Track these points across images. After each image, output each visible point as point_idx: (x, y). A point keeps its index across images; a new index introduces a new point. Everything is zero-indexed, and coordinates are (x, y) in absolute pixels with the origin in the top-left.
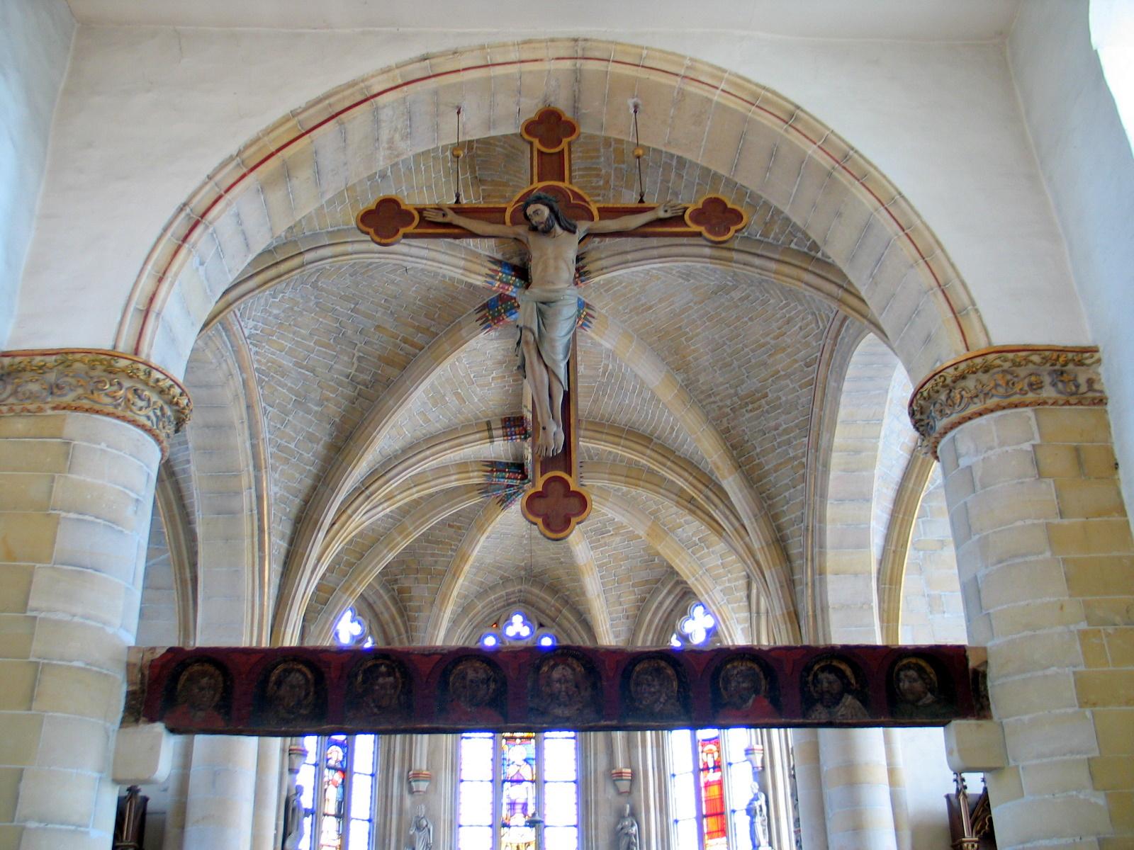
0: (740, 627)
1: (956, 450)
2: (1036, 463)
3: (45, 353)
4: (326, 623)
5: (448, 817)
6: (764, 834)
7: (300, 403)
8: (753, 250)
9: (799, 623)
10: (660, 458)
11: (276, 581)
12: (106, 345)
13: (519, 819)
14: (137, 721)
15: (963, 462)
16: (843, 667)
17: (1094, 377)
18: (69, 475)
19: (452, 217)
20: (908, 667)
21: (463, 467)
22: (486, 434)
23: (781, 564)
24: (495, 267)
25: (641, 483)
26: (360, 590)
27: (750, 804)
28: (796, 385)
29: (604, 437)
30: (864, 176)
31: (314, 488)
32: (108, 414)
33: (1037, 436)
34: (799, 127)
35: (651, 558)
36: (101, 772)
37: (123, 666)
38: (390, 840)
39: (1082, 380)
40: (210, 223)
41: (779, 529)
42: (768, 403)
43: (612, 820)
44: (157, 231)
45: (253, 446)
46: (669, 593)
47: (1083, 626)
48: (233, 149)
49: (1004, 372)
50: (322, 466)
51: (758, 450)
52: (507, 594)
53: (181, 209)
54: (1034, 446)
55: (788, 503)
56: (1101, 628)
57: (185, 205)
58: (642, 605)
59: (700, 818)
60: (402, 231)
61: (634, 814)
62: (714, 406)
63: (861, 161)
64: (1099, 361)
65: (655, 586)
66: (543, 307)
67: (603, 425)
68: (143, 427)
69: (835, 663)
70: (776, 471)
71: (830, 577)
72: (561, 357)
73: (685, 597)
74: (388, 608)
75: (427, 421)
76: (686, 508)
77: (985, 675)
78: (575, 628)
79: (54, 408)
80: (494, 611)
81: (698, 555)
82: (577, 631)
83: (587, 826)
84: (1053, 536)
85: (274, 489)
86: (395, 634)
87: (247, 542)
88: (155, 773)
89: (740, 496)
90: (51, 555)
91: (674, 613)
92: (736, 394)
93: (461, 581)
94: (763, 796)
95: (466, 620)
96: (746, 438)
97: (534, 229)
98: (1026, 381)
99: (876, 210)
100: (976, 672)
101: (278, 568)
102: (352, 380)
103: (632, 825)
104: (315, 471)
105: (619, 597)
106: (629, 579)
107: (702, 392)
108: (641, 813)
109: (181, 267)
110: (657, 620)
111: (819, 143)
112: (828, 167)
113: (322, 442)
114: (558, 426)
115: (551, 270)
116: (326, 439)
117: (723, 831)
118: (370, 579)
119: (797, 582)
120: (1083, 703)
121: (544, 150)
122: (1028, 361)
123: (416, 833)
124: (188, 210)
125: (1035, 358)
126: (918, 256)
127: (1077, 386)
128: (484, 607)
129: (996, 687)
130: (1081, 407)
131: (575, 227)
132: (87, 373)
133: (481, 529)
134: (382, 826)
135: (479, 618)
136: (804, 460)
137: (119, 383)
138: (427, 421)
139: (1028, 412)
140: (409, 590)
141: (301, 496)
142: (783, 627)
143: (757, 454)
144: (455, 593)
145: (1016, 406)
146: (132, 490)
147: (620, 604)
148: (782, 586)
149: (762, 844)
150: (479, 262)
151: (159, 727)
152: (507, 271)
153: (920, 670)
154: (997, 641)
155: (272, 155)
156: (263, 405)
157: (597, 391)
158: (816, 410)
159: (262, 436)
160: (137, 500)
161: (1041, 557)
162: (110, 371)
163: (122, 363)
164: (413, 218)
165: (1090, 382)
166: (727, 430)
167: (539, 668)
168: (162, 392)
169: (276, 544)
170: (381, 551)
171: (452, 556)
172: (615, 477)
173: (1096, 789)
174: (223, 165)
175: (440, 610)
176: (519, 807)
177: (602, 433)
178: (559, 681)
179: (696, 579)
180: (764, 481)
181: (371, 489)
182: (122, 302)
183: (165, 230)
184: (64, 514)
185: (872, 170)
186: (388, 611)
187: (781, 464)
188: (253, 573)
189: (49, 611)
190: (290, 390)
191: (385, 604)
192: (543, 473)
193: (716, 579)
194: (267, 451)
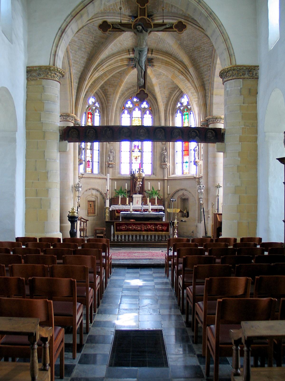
0: (195, 103)
1: (226, 86)
2: (241, 92)
3: (36, 67)
4: (86, 101)
5: (118, 149)
6: (197, 156)
7: (80, 49)
8: (194, 22)
9: (206, 106)
10: (174, 60)
11: (75, 94)
12: (47, 64)
13: (136, 150)
14: (62, 140)
15: (227, 89)
16: (197, 131)
17: (257, 72)
18: (45, 93)
19: (120, 27)
20: (209, 132)
21: (122, 60)
22: (128, 53)
23: (203, 91)
24: (130, 18)
25: (169, 66)
26: (95, 92)
27: (194, 149)
28: (209, 46)
29: (159, 54)
30: (215, 19)
31: (84, 70)
32: (51, 80)
33: (242, 86)
34: (201, 4)
35: (173, 83)
36: (57, 150)
37: (59, 130)
39: (254, 73)
40: (66, 32)
41: (203, 82)
42: (202, 50)
43: (161, 151)
44: (55, 35)
45: (68, 61)
46: (178, 91)
47: (243, 126)
48: (69, 13)
49: (238, 71)
50: (86, 64)
51: (199, 61)
52: (134, 90)
53: (59, 29)
54: (241, 88)
55: (206, 75)
56: (246, 127)
57: (60, 28)
58: (170, 94)
60: (108, 30)
61: (166, 149)
62: (188, 49)
63: (214, 15)
64: (259, 69)
65: (174, 89)
66: (140, 52)
67: (159, 51)
68: (57, 81)
69: (195, 130)
70: (203, 67)
71: (214, 96)
72: (143, 64)
73: (181, 95)
74: (102, 95)
75: (112, 50)
76: (181, 73)
77: (224, 134)
78: (152, 99)
79: (40, 79)
80: (130, 94)
81: (185, 83)
82: (153, 101)
83: (154, 152)
84: (241, 107)
85: (74, 71)
86: (104, 101)
87: (68, 85)
89: (193, 73)
90: (44, 110)
91: (179, 97)
92: (193, 47)
93: (122, 87)
94: (198, 147)
95: (123, 98)
96: (196, 58)
97: (138, 31)
98: (242, 73)
99: (216, 28)
100: (223, 133)
101: (76, 91)
102: (93, 42)
103: (165, 152)
104: (84, 66)
105: (164, 92)
106: (167, 87)
107: (185, 46)
109: (61, 43)
110: (174, 99)
111: (205, 9)
112: (207, 16)
113: (85, 58)
114: (143, 79)
115: (142, 42)
116: (86, 57)
117: (188, 155)
118: (98, 88)
119: (207, 96)
120: (240, 141)
121: (141, 7)
122: (243, 69)
124: (61, 29)
125: (244, 68)
126: (224, 41)
127: (253, 75)
128: (127, 94)
129: (226, 137)
130: (253, 79)
131: (147, 30)
132: (45, 71)
133: (127, 74)
135: (126, 97)
136: (210, 65)
137: (52, 73)
138: (112, 50)
139: (241, 80)
140: (107, 89)
141: (81, 72)
142: (202, 107)
143: (199, 62)
144: (120, 91)
145: (239, 79)
146: (56, 95)
147: (164, 94)
148: (203, 97)
150: (126, 17)
151: (67, 142)
152: (133, 19)
153: (212, 133)
154: (227, 128)
155: (78, 13)
156: (71, 50)
157: (158, 42)
158: (213, 53)
159: (70, 58)
160: (58, 97)
161: (238, 112)
162: (50, 70)
163: (52, 68)
164: (111, 27)
165: (256, 74)
166: (191, 56)
167: (138, 130)
168: (60, 73)
169: (75, 85)
170: (100, 81)
171: (119, 81)
172: (162, 63)
173: (239, 157)
174: (67, 17)
175: (116, 95)
176: (136, 147)
177: (159, 53)
178: (142, 132)
179: (184, 90)
180: (200, 69)
181: (98, 69)
182: (50, 53)
183: (57, 35)
184: (45, 102)
185: (216, 17)
186: (102, 95)
187: (204, 65)
188: (70, 93)
189: (45, 121)
190: (77, 46)
191: (101, 93)
192: (139, 89)
193: (190, 90)
194: (72, 62)
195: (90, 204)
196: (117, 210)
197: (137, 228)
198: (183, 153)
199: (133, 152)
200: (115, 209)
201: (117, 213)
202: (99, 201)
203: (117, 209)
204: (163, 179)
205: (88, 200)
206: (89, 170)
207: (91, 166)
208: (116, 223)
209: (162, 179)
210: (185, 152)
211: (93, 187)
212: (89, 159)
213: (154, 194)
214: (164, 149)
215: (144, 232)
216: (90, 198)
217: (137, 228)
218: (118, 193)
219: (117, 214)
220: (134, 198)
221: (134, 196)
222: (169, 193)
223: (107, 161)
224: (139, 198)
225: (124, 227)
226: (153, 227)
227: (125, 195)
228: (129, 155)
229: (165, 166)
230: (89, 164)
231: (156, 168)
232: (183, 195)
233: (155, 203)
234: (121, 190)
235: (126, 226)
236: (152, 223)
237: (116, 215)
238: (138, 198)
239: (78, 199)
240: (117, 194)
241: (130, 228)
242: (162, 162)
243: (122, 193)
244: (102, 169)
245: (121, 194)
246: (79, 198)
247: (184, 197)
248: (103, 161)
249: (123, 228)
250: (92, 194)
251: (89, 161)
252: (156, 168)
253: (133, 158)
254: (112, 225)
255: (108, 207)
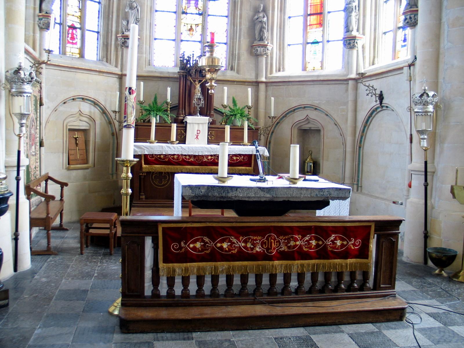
38: (112, 16)
43: (251, 13)
59: (307, 15)
61: (265, 10)
88: (135, 130)
103: (264, 17)
108: (269, 10)
123: (130, 11)
134: (107, 7)
149: (354, 30)
195: (76, 139)
196: (146, 156)
197: (249, 245)
198: (306, 21)
199: (184, 15)
200: (140, 154)
201: (145, 164)
202: (98, 130)
203: (146, 153)
204: (255, 80)
205: (69, 127)
206: (72, 50)
207: (78, 40)
208: (163, 228)
209: (253, 82)
210: (313, 19)
211: (84, 93)
212: (72, 20)
213: (239, 115)
214: (262, 8)
215: (276, 262)
216: (75, 124)
217: (249, 245)
218: (149, 111)
219: (147, 166)
220: (188, 126)
221: (189, 119)
222: (273, 115)
223: (120, 29)
224: (201, 125)
225: (198, 245)
226: (314, 243)
227: (165, 117)
228: (175, 21)
229: (262, 49)
230: (73, 34)
231: (239, 54)
232: (307, 120)
233: (242, 139)
234: (156, 103)
235: (207, 240)
236: (310, 227)
237: (144, 170)
238: (198, 124)
239: (22, 125)
240: (145, 113)
241: (221, 248)
242: (255, 40)
243: (159, 110)
244: (107, 51)
245: (157, 115)
246: (24, 121)
247: (307, 127)
248: (110, 31)
249: (194, 249)
250: (81, 113)
251: (73, 27)
252: (239, 54)
253: (184, 29)
254: (148, 234)
255: (131, 161)
